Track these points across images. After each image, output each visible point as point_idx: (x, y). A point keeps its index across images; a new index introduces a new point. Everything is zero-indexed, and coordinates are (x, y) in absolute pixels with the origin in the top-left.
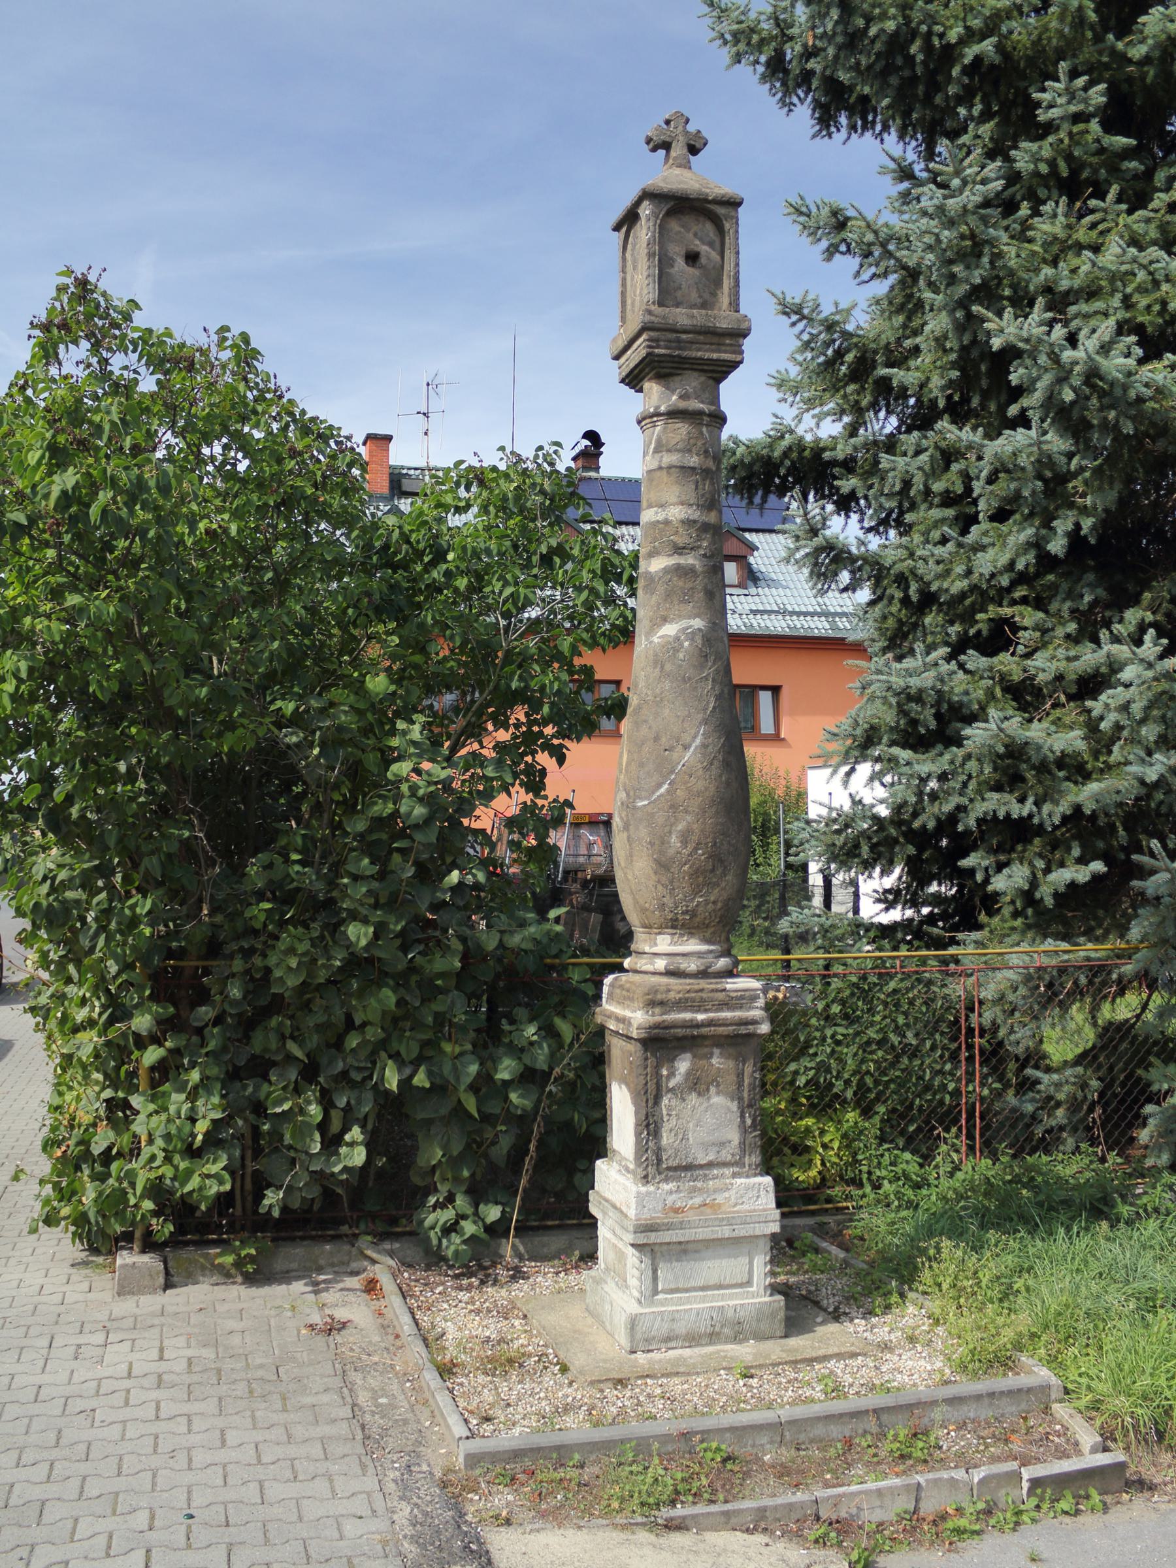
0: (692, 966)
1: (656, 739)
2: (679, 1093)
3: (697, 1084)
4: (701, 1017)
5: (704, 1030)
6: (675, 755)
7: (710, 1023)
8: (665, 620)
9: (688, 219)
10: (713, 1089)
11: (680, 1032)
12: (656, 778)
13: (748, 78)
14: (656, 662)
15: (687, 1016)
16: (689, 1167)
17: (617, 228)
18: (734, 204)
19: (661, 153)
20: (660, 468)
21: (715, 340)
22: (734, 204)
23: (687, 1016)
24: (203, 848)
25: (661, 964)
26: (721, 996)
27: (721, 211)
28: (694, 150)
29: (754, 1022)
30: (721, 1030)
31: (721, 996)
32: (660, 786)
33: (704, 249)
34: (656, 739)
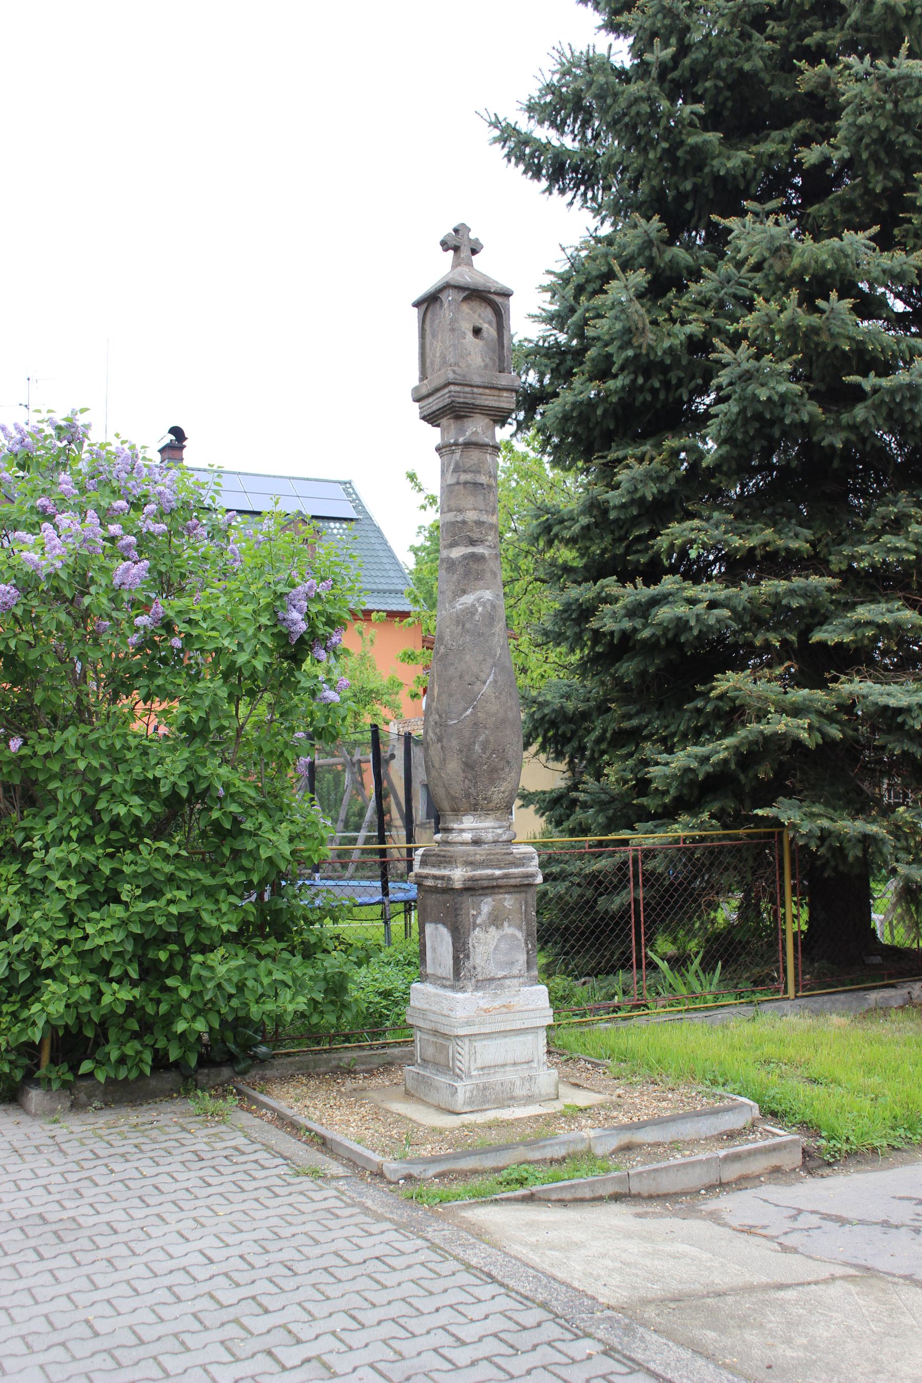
0: (489, 837)
1: (461, 677)
2: (485, 927)
3: (496, 920)
4: (498, 872)
5: (501, 882)
6: (476, 688)
7: (506, 876)
8: (464, 592)
9: (475, 304)
10: (506, 924)
11: (485, 883)
12: (462, 704)
13: (499, 151)
14: (458, 622)
15: (489, 872)
16: (492, 979)
17: (417, 305)
18: (507, 294)
19: (451, 252)
20: (458, 483)
21: (496, 393)
22: (507, 294)
23: (489, 872)
24: (748, 835)
25: (467, 836)
26: (510, 858)
27: (498, 299)
28: (474, 252)
29: (533, 876)
30: (512, 882)
31: (510, 858)
32: (466, 709)
33: (485, 326)
34: (461, 677)
